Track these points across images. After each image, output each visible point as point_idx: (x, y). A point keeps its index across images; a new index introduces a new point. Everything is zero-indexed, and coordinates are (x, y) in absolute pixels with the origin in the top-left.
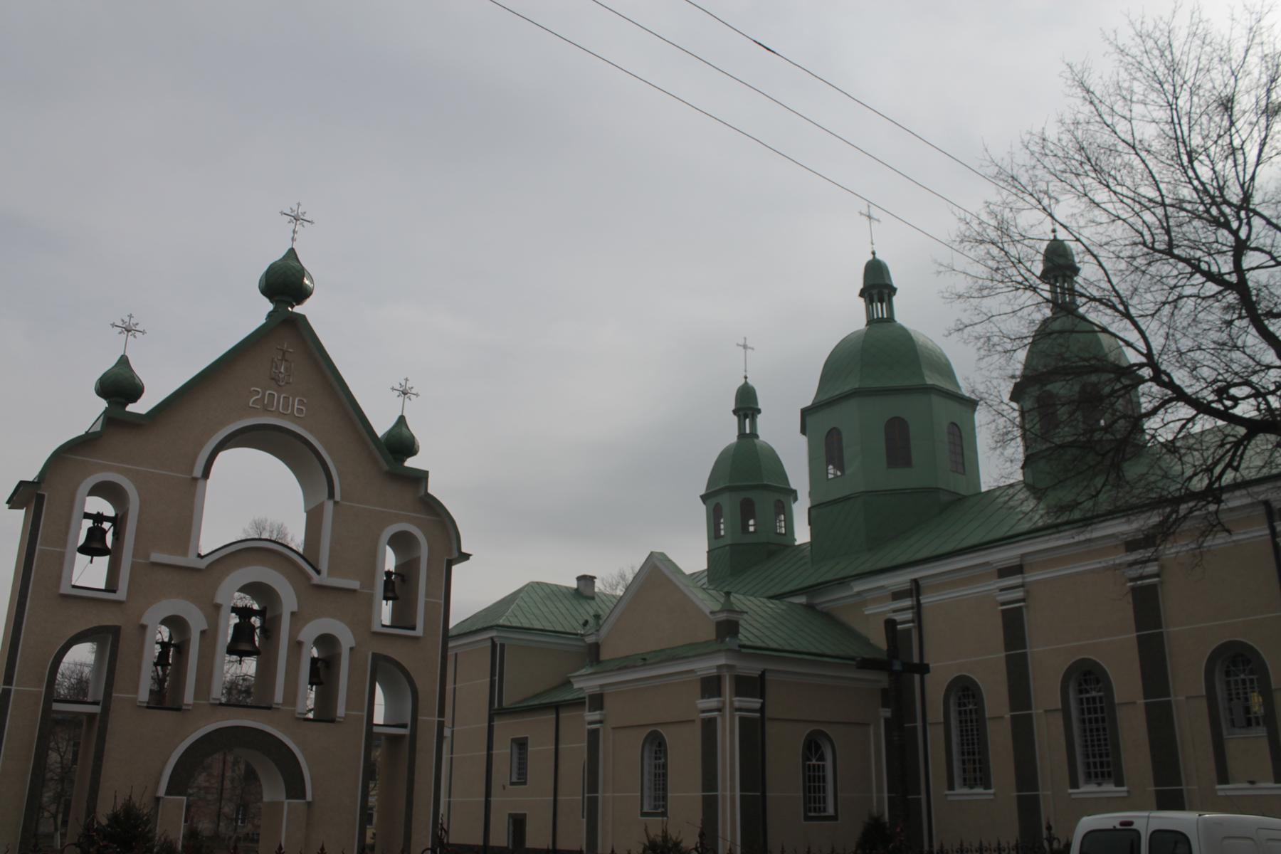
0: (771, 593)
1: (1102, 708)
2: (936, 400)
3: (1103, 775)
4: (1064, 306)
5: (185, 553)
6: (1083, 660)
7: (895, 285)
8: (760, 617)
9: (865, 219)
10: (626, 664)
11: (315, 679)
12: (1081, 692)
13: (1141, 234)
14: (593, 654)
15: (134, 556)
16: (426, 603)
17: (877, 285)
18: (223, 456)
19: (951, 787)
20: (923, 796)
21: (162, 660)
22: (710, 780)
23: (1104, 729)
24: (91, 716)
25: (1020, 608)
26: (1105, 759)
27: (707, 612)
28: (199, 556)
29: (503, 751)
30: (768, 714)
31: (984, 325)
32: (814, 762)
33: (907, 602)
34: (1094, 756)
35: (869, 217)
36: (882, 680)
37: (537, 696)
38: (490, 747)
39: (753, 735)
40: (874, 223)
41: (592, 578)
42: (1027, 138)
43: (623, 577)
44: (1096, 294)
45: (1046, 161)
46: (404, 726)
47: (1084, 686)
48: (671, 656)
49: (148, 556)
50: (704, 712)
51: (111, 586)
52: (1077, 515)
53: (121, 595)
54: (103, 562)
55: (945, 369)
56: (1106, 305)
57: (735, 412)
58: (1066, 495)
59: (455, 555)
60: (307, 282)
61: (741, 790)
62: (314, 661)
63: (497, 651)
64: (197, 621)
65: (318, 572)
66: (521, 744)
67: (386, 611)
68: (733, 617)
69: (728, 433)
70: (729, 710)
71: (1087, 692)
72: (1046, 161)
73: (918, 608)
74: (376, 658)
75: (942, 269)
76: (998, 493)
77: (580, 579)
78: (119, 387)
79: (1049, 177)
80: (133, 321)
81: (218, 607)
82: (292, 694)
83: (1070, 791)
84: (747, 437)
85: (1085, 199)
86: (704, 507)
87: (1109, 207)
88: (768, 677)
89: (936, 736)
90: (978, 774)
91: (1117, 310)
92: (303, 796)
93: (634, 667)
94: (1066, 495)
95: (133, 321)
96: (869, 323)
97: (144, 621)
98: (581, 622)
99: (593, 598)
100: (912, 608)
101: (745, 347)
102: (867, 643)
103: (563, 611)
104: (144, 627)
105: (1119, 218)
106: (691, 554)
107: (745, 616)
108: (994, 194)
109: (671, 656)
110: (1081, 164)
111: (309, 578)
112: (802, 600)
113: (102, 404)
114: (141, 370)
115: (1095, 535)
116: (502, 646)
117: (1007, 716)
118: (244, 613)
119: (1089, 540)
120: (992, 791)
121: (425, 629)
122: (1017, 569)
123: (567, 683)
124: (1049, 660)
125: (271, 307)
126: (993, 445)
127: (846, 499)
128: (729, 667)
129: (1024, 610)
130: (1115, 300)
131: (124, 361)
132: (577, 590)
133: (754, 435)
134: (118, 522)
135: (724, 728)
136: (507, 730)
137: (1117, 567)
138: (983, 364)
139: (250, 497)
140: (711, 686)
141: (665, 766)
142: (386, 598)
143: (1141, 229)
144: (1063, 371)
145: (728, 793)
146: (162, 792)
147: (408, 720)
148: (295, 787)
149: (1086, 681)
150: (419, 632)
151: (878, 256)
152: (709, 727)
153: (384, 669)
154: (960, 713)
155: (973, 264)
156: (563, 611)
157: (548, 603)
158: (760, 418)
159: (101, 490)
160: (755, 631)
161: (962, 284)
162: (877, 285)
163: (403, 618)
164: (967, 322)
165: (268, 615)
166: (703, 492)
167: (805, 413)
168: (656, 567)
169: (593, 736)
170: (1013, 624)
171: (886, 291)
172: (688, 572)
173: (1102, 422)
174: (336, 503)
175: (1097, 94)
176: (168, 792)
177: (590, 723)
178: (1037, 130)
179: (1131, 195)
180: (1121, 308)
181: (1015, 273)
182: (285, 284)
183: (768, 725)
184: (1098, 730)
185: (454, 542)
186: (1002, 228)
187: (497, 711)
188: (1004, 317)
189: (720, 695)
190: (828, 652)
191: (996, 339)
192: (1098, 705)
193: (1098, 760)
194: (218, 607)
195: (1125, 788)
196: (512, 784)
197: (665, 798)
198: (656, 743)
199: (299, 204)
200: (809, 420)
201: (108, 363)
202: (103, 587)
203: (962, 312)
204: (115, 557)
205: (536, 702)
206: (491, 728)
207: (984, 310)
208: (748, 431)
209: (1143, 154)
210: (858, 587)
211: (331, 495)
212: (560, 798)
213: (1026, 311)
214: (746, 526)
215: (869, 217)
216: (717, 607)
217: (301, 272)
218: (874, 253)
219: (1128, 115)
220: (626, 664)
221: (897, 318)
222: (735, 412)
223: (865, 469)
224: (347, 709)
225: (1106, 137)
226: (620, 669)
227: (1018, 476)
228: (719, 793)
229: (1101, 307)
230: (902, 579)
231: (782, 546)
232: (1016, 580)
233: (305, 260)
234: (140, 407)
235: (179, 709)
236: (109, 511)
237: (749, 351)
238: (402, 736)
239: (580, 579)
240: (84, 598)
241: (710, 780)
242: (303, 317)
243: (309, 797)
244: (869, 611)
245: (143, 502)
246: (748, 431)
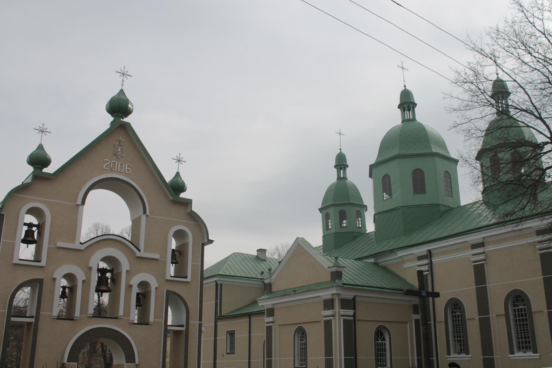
0: (356, 257)
1: (525, 314)
2: (438, 160)
3: (526, 348)
4: (503, 113)
5: (73, 242)
6: (515, 290)
7: (416, 102)
8: (353, 270)
9: (401, 69)
10: (285, 293)
11: (139, 303)
12: (514, 306)
13: (548, 78)
14: (267, 288)
15: (49, 244)
16: (192, 265)
17: (407, 103)
18: (92, 193)
19: (449, 354)
20: (435, 358)
21: (63, 295)
22: (329, 351)
23: (527, 325)
24: (29, 324)
25: (483, 264)
26: (527, 340)
27: (326, 267)
28: (81, 243)
29: (222, 337)
30: (357, 318)
31: (467, 124)
32: (380, 341)
33: (426, 261)
34: (522, 338)
35: (403, 68)
36: (416, 300)
37: (239, 309)
38: (216, 336)
39: (350, 328)
40: (405, 71)
41: (264, 251)
42: (489, 30)
43: (277, 249)
44: (524, 108)
45: (500, 41)
46: (182, 326)
47: (516, 303)
48: (308, 289)
49: (56, 244)
50: (325, 317)
51: (37, 258)
52: (514, 217)
53: (43, 263)
54: (33, 247)
55: (442, 145)
56: (528, 112)
57: (335, 167)
58: (509, 207)
59: (206, 241)
60: (130, 106)
61: (417, 356)
62: (138, 294)
63: (218, 287)
64: (80, 276)
65: (139, 251)
66: (232, 334)
67: (172, 270)
68: (339, 269)
69: (332, 177)
70: (338, 317)
71: (518, 306)
72: (500, 41)
73: (431, 264)
74: (168, 292)
75: (446, 96)
76: (469, 207)
77: (258, 251)
78: (39, 160)
79: (500, 49)
80: (45, 127)
81: (90, 268)
82: (127, 312)
83: (510, 356)
84: (342, 179)
85: (520, 61)
86: (321, 214)
87: (531, 64)
88: (357, 299)
89: (441, 328)
90: (464, 348)
91: (535, 116)
92: (134, 362)
93: (290, 295)
94: (509, 207)
95: (45, 127)
96: (403, 122)
97: (55, 276)
98: (260, 272)
99: (265, 260)
100: (428, 264)
101: (340, 134)
102: (405, 281)
103: (251, 267)
104: (54, 279)
105: (536, 69)
106: (316, 239)
107: (345, 269)
108: (472, 57)
109: (308, 289)
110: (517, 42)
111: (134, 253)
112: (372, 260)
113: (31, 169)
114: (50, 151)
115: (524, 226)
116: (221, 285)
117: (477, 318)
118: (103, 271)
119: (520, 230)
120: (470, 356)
121: (191, 278)
122: (482, 245)
123: (255, 302)
124: (498, 291)
125: (112, 119)
126: (473, 183)
127: (393, 210)
128: (338, 294)
129: (485, 265)
130: (534, 111)
131: (41, 147)
132: (257, 256)
133: (345, 178)
134: (40, 227)
135: (335, 325)
136: (224, 327)
137: (534, 244)
138: (467, 143)
139: (105, 213)
140: (328, 304)
141: (305, 344)
142: (172, 263)
143: (547, 75)
144: (505, 145)
145: (338, 357)
146: (65, 361)
147: (184, 323)
148: (130, 358)
149: (517, 300)
150: (189, 279)
151: (407, 88)
152: (328, 325)
153: (172, 298)
154: (453, 316)
155: (461, 94)
156: (251, 267)
157: (243, 263)
158: (348, 170)
159: (33, 211)
160: (349, 276)
161: (456, 104)
162: (407, 103)
163: (181, 273)
164: (459, 122)
165: (115, 272)
166: (320, 207)
167: (372, 167)
168: (299, 245)
169: (269, 329)
170: (479, 272)
171: (412, 105)
172: (314, 246)
173: (523, 171)
174: (147, 216)
175: (525, 7)
176: (68, 361)
177: (267, 323)
178: (494, 26)
179: (543, 58)
180: (536, 114)
181: (484, 98)
182: (119, 108)
183: (357, 323)
184: (456, 321)
185: (205, 235)
186: (476, 74)
187: (219, 317)
188: (477, 120)
189: (333, 309)
190: (387, 287)
191: (473, 131)
192: (523, 312)
193: (524, 340)
194: (90, 268)
195: (538, 354)
196: (227, 354)
197: (306, 360)
198: (301, 333)
199: (124, 67)
200: (374, 171)
201: (32, 148)
202: (33, 259)
203: (456, 117)
204: (38, 243)
205: (239, 313)
206: (216, 326)
207: (468, 117)
208: (342, 176)
209: (548, 36)
210: (400, 254)
211: (145, 212)
212: (251, 360)
213: (484, 116)
214: (341, 223)
215: (403, 68)
216: (331, 265)
217: (127, 101)
218: (405, 86)
219: (540, 17)
220: (285, 293)
221: (417, 119)
222: (335, 167)
223: (403, 195)
224: (154, 318)
225: (530, 29)
226: (282, 296)
227: (480, 197)
228: (334, 357)
229: (527, 115)
230: (422, 250)
231: (358, 234)
232: (481, 250)
233: (129, 95)
234: (50, 170)
235: (72, 319)
236: (35, 222)
237: (342, 136)
238: (182, 331)
239: (258, 251)
240: (23, 265)
241: (329, 351)
242: (129, 124)
243: (137, 362)
244: (405, 266)
245: (52, 217)
246: (342, 176)
